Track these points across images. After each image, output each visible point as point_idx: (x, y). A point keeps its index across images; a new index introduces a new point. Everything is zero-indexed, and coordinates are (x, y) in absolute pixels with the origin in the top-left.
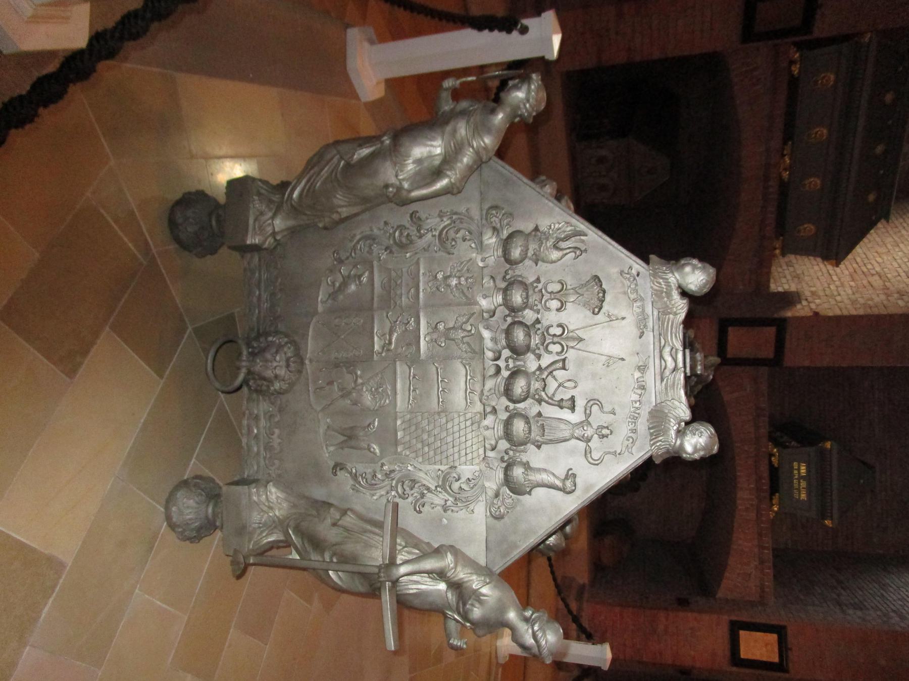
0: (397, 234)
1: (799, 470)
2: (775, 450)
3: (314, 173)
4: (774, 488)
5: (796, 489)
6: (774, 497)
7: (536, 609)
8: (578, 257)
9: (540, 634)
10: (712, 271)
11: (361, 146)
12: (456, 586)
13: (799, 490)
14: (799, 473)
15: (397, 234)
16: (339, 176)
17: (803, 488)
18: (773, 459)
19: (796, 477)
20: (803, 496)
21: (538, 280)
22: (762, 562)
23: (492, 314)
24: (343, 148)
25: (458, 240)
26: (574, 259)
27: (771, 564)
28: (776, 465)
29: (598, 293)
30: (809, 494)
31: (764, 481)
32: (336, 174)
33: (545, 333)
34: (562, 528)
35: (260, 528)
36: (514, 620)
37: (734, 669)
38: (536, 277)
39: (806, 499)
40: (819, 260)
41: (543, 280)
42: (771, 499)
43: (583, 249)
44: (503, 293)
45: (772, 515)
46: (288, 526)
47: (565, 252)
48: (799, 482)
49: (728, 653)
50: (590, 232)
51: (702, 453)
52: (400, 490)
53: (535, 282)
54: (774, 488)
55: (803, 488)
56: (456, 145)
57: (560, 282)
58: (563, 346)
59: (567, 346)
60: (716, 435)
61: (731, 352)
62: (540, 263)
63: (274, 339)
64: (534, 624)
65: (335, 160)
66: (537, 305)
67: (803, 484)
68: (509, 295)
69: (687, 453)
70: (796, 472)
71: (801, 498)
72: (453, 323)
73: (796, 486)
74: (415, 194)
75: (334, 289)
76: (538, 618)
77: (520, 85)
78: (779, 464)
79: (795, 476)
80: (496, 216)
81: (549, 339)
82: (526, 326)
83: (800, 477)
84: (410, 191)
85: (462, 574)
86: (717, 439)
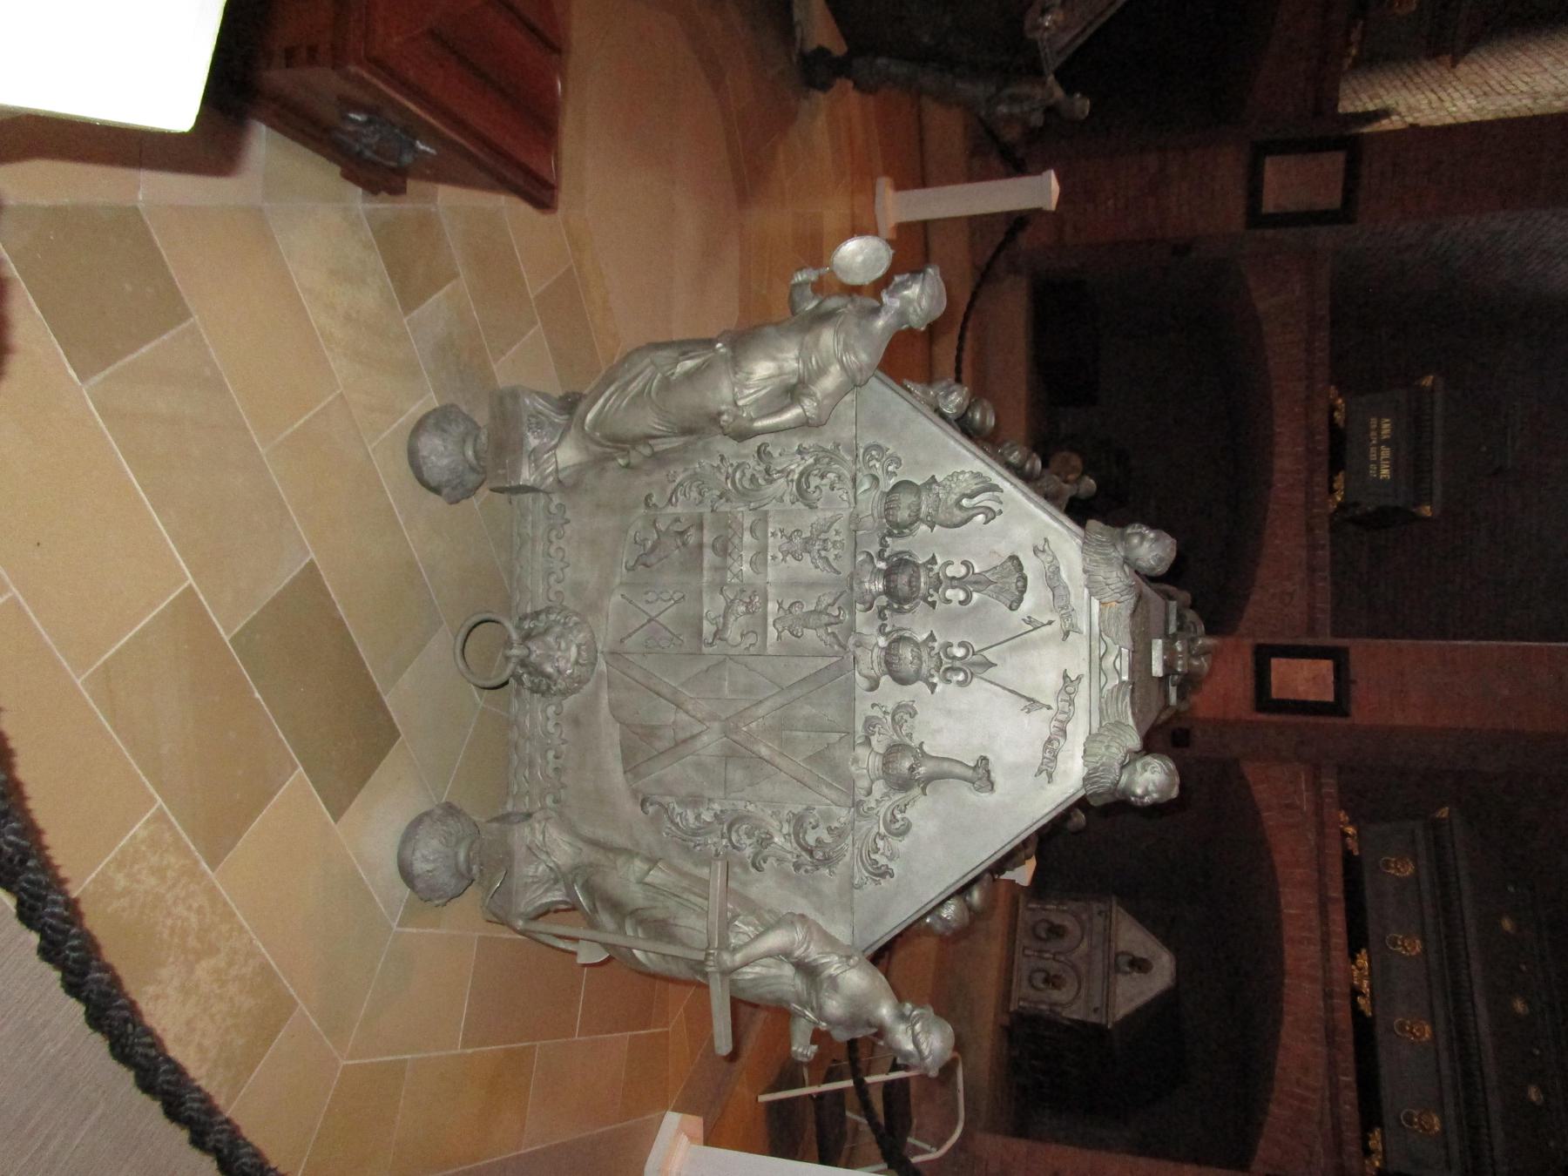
0: (738, 475)
1: (1379, 429)
2: (1340, 401)
3: (619, 387)
4: (1337, 462)
5: (1374, 462)
6: (1336, 478)
7: (917, 1004)
8: (989, 521)
9: (921, 1038)
10: (1154, 675)
11: (685, 355)
12: (807, 970)
13: (1377, 463)
14: (1379, 434)
15: (738, 475)
16: (653, 394)
17: (1384, 460)
18: (1336, 414)
19: (1374, 442)
20: (1385, 472)
21: (933, 560)
22: (1312, 570)
23: (868, 605)
24: (663, 356)
25: (823, 488)
26: (985, 524)
27: (1327, 573)
28: (1342, 424)
29: (1018, 581)
30: (1394, 469)
31: (1318, 437)
32: (649, 392)
33: (942, 654)
34: (963, 891)
35: (533, 883)
36: (887, 1018)
37: (1262, 717)
38: (930, 632)
39: (1389, 477)
40: (1426, 64)
41: (940, 561)
42: (1331, 481)
43: (996, 510)
44: (884, 578)
45: (1332, 507)
46: (574, 881)
47: (971, 512)
48: (1379, 451)
49: (1250, 693)
50: (1006, 486)
51: (1155, 796)
52: (734, 838)
53: (929, 562)
54: (1337, 462)
55: (1384, 460)
56: (820, 362)
57: (965, 563)
58: (966, 674)
59: (972, 674)
60: (1176, 772)
61: (1269, 205)
62: (937, 528)
63: (558, 617)
64: (915, 1024)
65: (648, 372)
66: (932, 596)
67: (1386, 452)
68: (893, 581)
69: (1135, 796)
70: (1373, 434)
71: (1381, 477)
72: (814, 605)
73: (1373, 457)
74: (759, 424)
75: (644, 550)
76: (921, 1017)
77: (910, 283)
78: (1346, 421)
79: (1371, 441)
80: (877, 460)
81: (947, 663)
82: (917, 644)
83: (1381, 442)
84: (752, 420)
85: (814, 953)
86: (1177, 780)
